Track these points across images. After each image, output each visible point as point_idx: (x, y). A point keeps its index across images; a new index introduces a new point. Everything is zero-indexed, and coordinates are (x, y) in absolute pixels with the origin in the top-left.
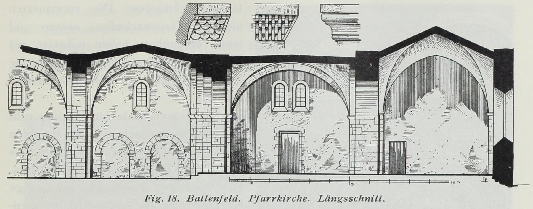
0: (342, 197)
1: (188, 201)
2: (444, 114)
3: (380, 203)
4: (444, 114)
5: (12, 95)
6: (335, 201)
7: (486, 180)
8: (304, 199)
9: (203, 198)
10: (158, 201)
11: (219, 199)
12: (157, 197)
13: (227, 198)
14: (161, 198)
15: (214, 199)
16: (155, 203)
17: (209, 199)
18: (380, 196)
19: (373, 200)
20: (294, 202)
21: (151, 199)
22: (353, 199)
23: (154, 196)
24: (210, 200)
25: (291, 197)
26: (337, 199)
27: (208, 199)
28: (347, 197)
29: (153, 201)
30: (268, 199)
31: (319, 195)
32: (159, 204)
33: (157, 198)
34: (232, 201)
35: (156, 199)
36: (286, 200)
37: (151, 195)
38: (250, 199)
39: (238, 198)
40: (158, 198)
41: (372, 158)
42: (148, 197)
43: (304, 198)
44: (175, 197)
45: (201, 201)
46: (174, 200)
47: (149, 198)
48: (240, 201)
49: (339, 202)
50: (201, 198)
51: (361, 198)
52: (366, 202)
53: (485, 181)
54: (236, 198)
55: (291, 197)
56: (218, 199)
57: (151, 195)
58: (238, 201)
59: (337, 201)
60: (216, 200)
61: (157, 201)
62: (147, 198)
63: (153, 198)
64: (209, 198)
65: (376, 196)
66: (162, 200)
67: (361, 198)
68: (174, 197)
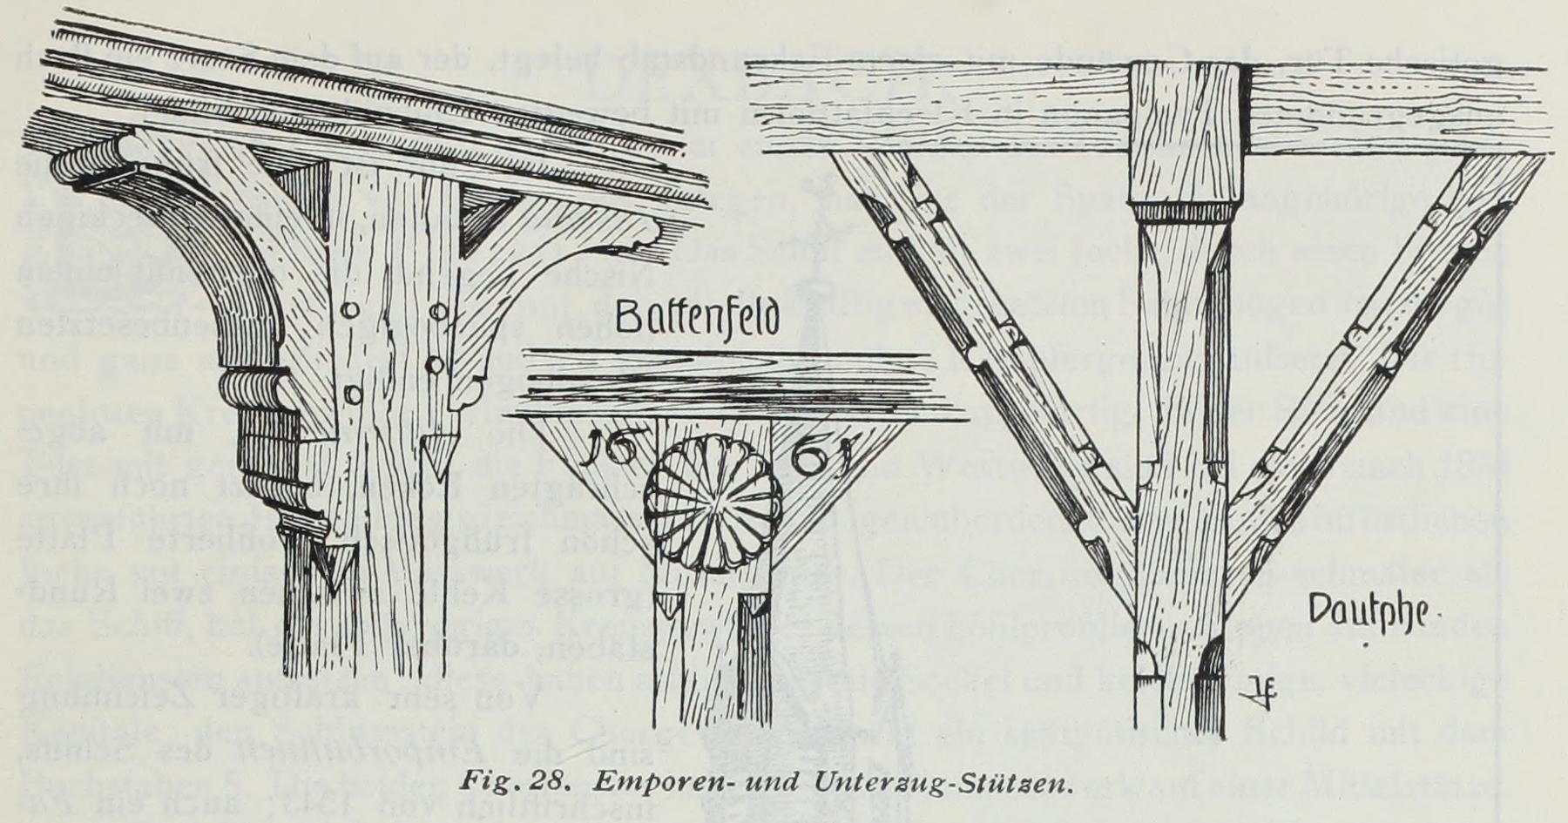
0: (943, 779)
1: (599, 787)
2: (676, 241)
3: (461, 793)
4: (676, 241)
5: (1408, 297)
6: (638, 787)
7: (1268, 687)
8: (1036, 786)
9: (1015, 782)
10: (936, 791)
11: (851, 784)
12: (497, 776)
13: (874, 781)
14: (509, 779)
15: (1050, 786)
16: (493, 794)
17: (868, 785)
18: (1010, 776)
19: (484, 781)
20: (699, 792)
21: (481, 781)
22: (1032, 785)
23: (491, 772)
24: (871, 788)
25: (689, 778)
26: (929, 785)
27: (863, 783)
28: (973, 775)
29: (485, 786)
30: (683, 782)
31: (596, 771)
32: (940, 799)
33: (934, 781)
34: (782, 788)
35: (496, 782)
36: (764, 787)
37: (482, 771)
38: (463, 782)
39: (798, 779)
40: (501, 780)
41: (1119, 581)
42: (473, 776)
43: (1038, 783)
44: (558, 775)
45: (1009, 790)
46: (554, 784)
47: (475, 780)
48: (1070, 791)
49: (935, 793)
50: (1008, 782)
51: (974, 784)
52: (619, 792)
53: (1263, 692)
54: (795, 780)
55: (689, 778)
56: (848, 784)
57: (482, 771)
58: (1066, 791)
59: (493, 787)
60: (919, 783)
61: (934, 789)
62: (601, 779)
63: (487, 778)
64: (866, 783)
65: (981, 776)
66: (516, 784)
67: (974, 784)
68: (553, 774)
